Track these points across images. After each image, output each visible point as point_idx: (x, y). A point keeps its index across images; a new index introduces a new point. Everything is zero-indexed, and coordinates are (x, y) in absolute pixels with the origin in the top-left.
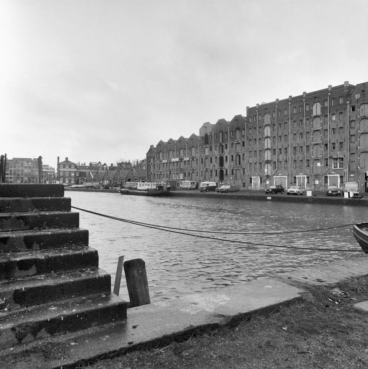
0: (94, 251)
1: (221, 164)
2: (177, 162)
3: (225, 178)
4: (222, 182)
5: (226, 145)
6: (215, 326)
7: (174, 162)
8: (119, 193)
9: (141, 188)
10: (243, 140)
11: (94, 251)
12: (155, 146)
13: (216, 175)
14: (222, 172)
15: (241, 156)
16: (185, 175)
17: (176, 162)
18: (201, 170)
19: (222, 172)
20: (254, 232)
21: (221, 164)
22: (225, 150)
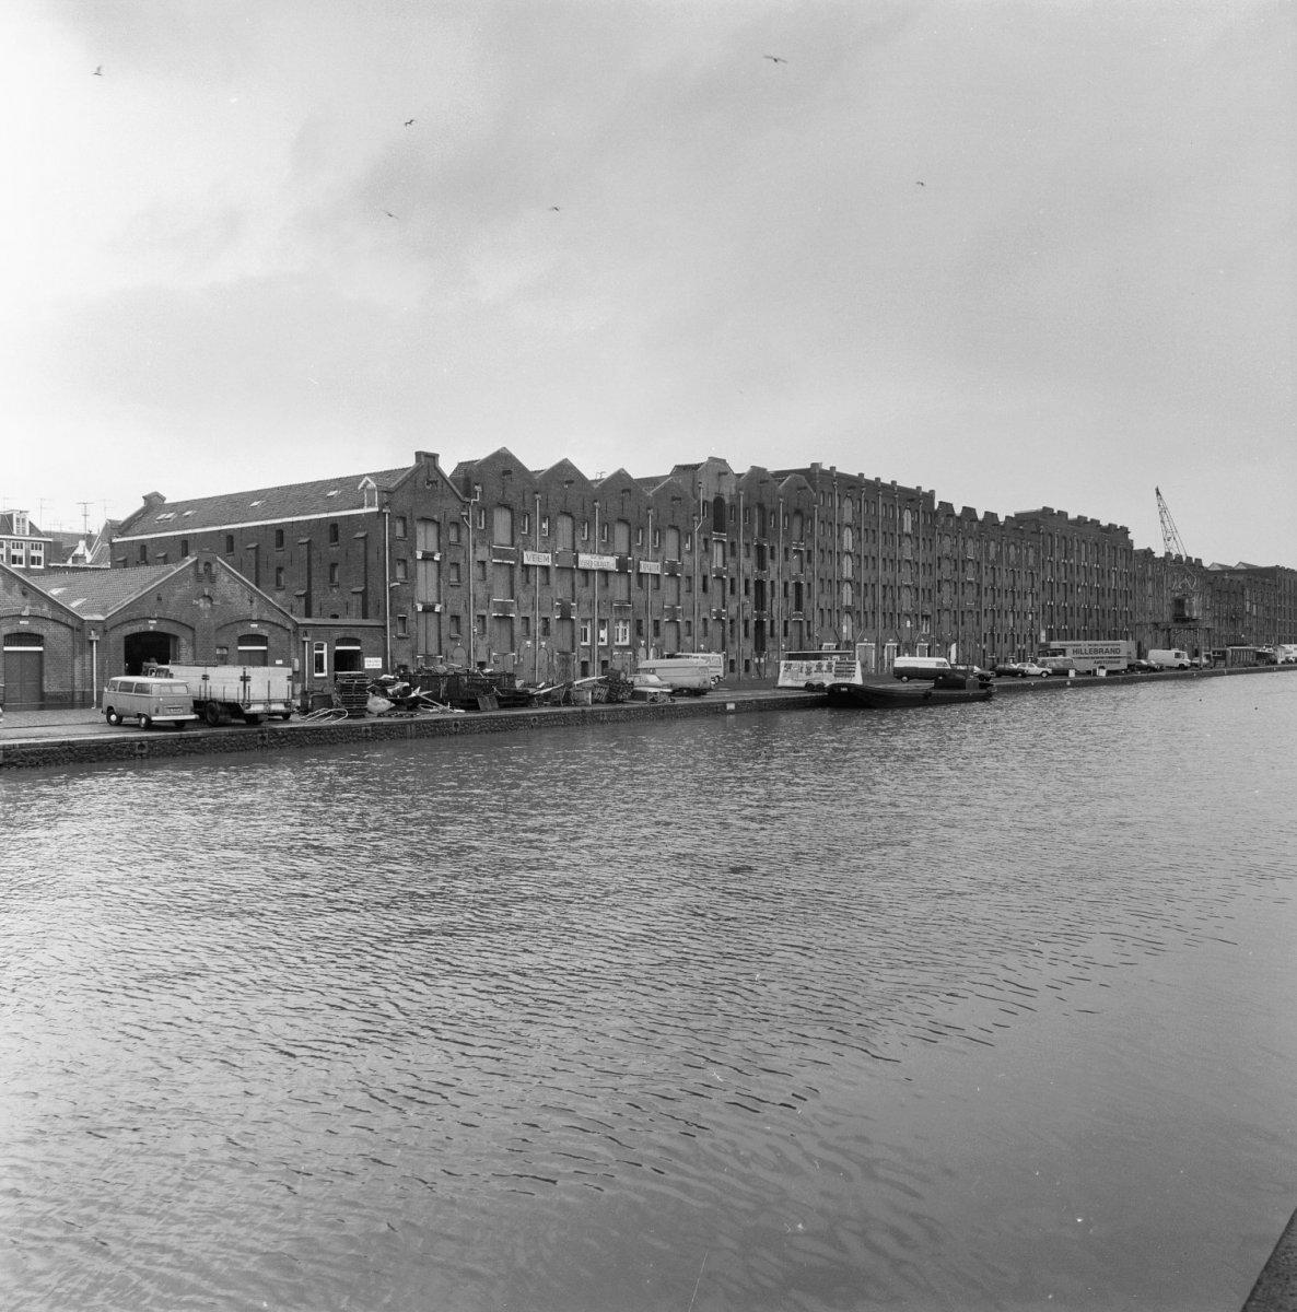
0: (1184, 559)
1: (760, 604)
2: (605, 573)
3: (769, 645)
4: (759, 656)
5: (772, 548)
6: (920, 678)
7: (586, 572)
8: (1069, 687)
9: (789, 683)
10: (809, 546)
11: (1184, 559)
12: (447, 467)
13: (746, 635)
14: (760, 625)
15: (805, 588)
16: (638, 630)
17: (600, 571)
18: (702, 616)
19: (760, 625)
20: (814, 993)
21: (760, 604)
22: (769, 563)
